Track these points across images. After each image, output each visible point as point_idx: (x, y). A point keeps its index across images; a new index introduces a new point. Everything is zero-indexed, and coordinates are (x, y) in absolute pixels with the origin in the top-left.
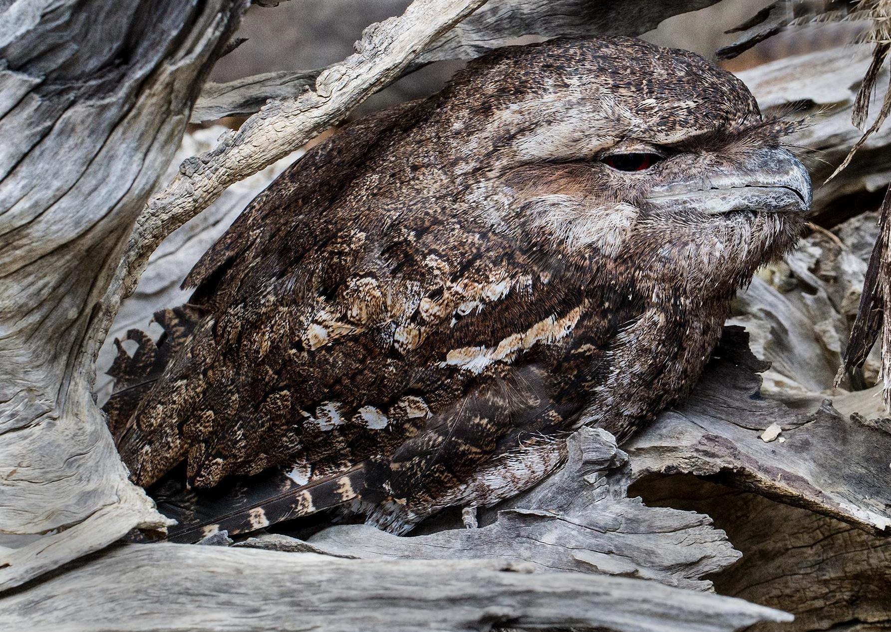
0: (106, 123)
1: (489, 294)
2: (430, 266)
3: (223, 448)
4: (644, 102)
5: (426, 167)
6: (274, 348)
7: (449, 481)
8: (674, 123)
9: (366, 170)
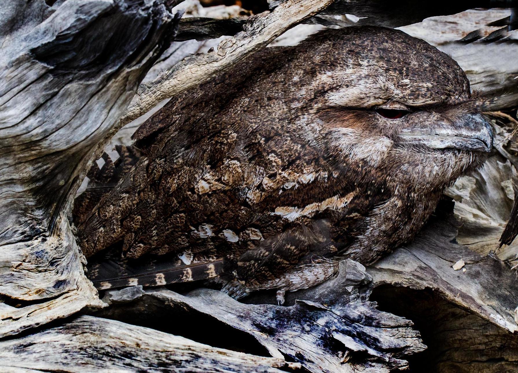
0: (89, 93)
1: (302, 180)
2: (271, 160)
3: (144, 239)
4: (403, 81)
5: (276, 100)
6: (178, 188)
7: (270, 276)
8: (419, 95)
9: (242, 94)
